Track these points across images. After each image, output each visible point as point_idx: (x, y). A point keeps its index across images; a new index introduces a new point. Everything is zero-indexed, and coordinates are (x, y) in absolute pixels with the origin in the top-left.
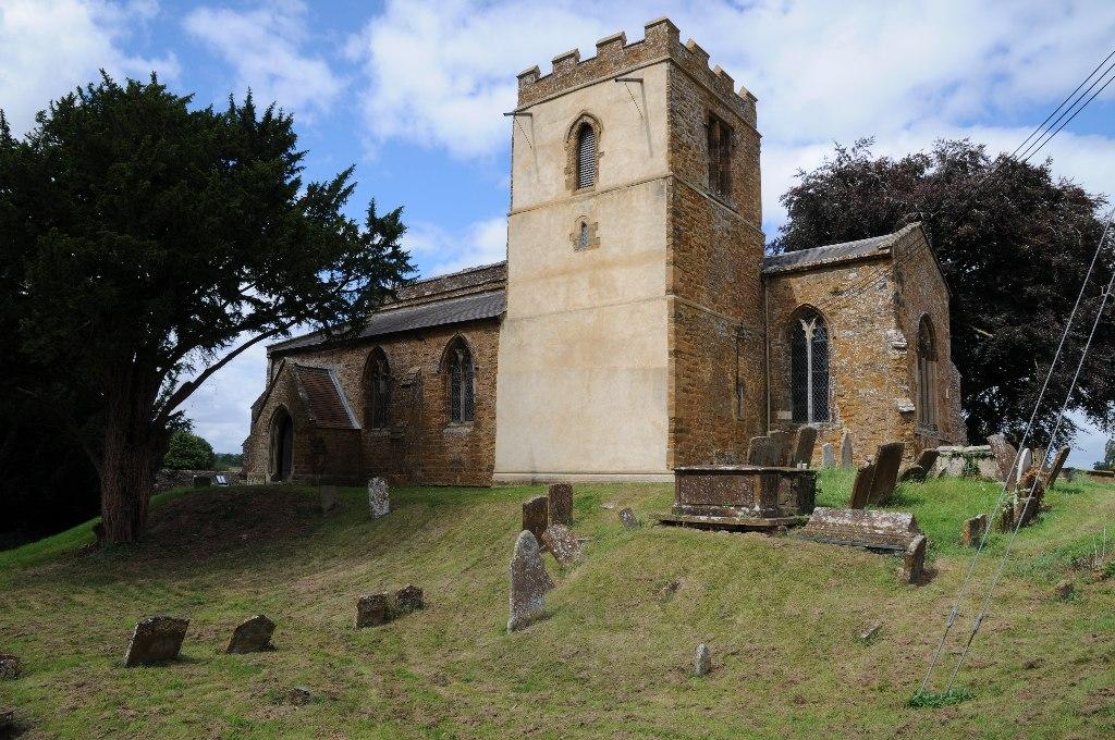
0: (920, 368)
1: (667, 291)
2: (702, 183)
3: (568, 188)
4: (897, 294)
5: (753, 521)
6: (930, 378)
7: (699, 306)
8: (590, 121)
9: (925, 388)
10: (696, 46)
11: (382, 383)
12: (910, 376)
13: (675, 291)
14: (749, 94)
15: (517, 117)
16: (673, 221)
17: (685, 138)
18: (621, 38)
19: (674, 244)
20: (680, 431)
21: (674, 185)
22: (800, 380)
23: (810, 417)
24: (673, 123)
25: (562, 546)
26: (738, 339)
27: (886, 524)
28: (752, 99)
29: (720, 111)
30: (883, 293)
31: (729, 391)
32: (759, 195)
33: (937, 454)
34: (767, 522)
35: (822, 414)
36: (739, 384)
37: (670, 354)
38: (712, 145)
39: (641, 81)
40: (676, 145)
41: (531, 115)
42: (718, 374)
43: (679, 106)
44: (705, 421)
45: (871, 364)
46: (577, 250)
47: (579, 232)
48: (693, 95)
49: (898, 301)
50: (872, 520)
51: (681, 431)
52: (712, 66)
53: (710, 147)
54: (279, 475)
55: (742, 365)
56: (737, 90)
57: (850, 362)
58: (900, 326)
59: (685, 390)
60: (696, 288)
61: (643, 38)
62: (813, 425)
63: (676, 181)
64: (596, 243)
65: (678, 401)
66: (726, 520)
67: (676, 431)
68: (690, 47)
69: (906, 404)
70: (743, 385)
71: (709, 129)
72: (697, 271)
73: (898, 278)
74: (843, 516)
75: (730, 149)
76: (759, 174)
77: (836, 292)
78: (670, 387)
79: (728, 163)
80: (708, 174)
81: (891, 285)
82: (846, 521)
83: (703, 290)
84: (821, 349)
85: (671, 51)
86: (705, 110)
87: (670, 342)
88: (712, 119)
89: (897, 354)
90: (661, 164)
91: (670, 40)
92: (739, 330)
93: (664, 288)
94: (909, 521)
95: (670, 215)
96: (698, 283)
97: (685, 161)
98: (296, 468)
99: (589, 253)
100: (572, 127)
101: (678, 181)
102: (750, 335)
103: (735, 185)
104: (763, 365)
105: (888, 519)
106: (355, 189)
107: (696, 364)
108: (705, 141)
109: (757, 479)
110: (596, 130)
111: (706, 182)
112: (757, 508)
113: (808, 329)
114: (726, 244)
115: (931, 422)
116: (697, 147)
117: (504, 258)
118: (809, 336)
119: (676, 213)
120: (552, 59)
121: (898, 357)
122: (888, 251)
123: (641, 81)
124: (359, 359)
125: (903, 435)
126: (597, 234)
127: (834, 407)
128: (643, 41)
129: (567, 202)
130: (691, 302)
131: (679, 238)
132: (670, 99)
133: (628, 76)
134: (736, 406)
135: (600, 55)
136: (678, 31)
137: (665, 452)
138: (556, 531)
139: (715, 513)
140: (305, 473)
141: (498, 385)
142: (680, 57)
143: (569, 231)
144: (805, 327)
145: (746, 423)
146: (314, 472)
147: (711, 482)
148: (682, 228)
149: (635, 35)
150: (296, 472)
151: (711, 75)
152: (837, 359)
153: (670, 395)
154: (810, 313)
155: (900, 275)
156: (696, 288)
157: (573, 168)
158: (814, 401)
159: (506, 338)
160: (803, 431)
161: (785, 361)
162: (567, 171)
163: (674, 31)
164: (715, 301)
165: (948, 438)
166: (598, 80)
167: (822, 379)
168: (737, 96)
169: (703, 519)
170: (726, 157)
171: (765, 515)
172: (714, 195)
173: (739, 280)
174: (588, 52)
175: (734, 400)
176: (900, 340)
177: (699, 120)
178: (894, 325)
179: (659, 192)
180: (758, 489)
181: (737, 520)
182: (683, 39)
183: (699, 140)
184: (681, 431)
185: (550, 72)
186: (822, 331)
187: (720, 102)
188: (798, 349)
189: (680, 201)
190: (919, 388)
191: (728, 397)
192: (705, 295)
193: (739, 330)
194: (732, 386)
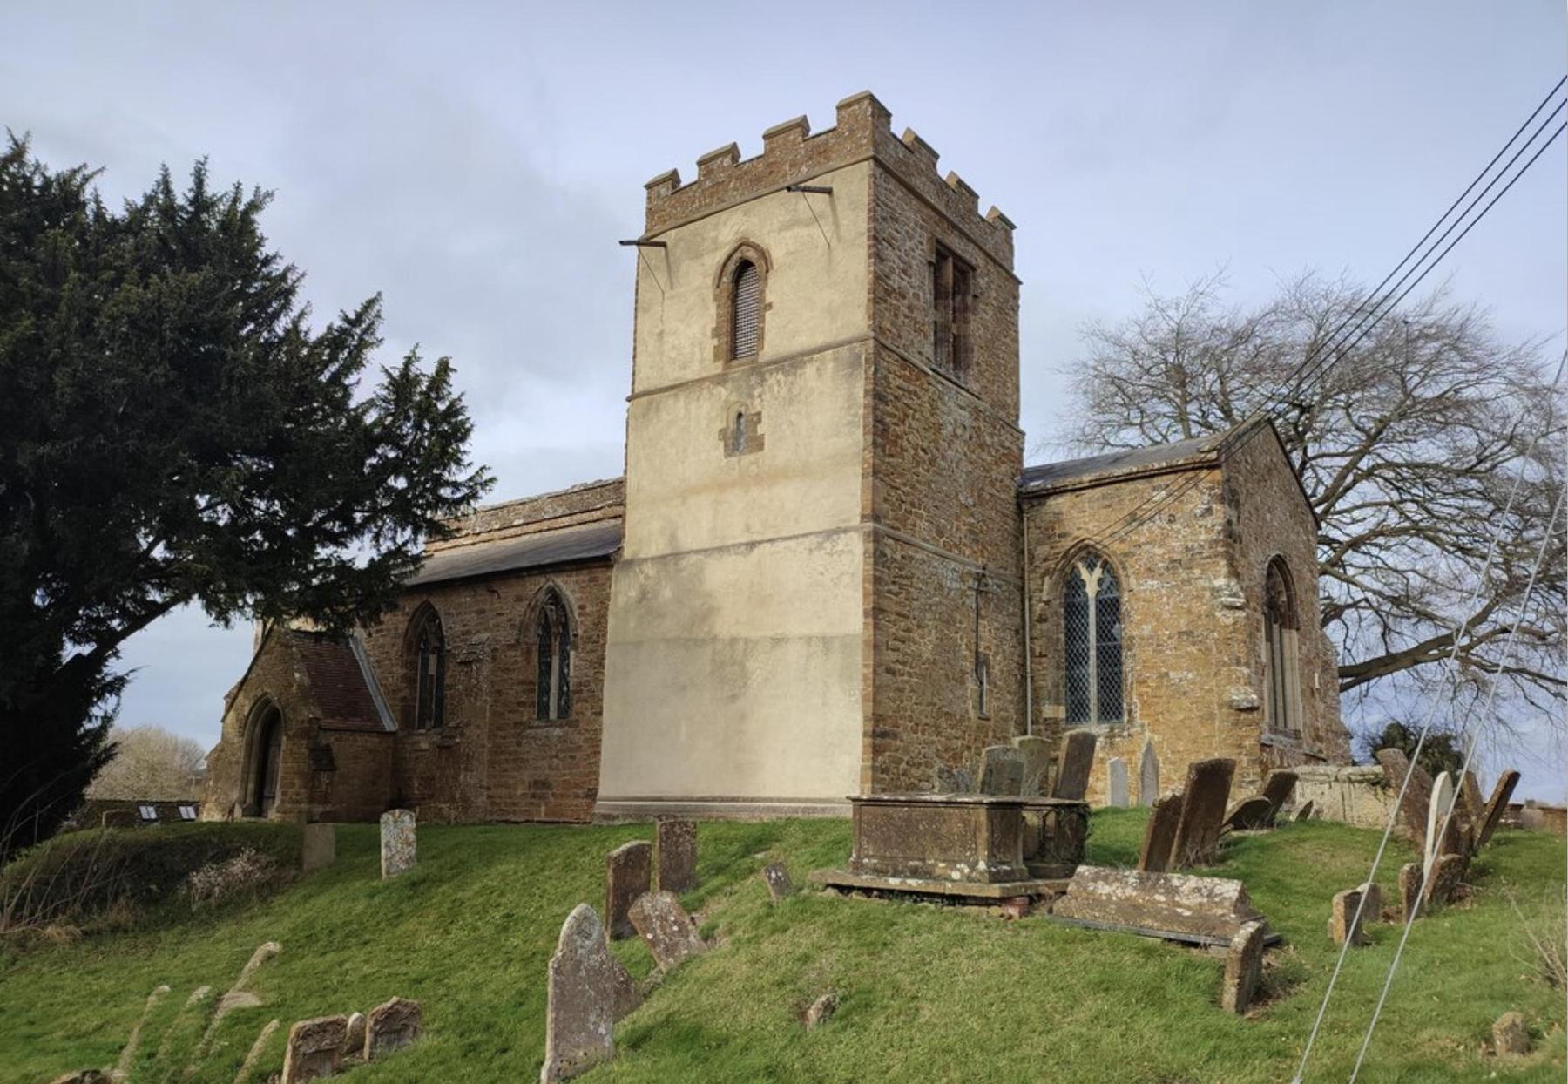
0: (1269, 639)
1: (863, 517)
2: (922, 350)
3: (716, 357)
4: (1229, 523)
5: (975, 890)
6: (1287, 655)
7: (914, 540)
8: (751, 254)
9: (1278, 671)
10: (917, 139)
11: (433, 659)
12: (1252, 650)
13: (876, 518)
14: (1002, 218)
15: (643, 248)
16: (875, 408)
17: (895, 282)
18: (802, 125)
19: (875, 444)
20: (880, 735)
21: (877, 354)
22: (1075, 658)
23: (1093, 714)
24: (877, 256)
25: (662, 927)
26: (979, 592)
27: (1196, 900)
28: (1004, 225)
29: (955, 242)
30: (1209, 521)
31: (964, 673)
32: (1015, 371)
33: (1293, 778)
34: (995, 891)
35: (1112, 708)
36: (980, 662)
37: (866, 614)
38: (939, 293)
39: (829, 192)
40: (882, 292)
41: (663, 245)
42: (946, 647)
43: (889, 229)
44: (925, 721)
45: (1189, 633)
46: (728, 454)
47: (732, 426)
48: (910, 213)
49: (1231, 535)
50: (1172, 891)
51: (884, 735)
52: (943, 171)
53: (936, 298)
54: (258, 805)
55: (984, 633)
56: (983, 211)
57: (1154, 630)
58: (1234, 573)
59: (890, 671)
60: (910, 512)
61: (835, 124)
62: (1094, 727)
63: (881, 346)
64: (757, 443)
65: (877, 689)
66: (932, 888)
67: (875, 735)
68: (907, 141)
69: (1242, 694)
70: (986, 662)
71: (936, 268)
72: (913, 487)
73: (1231, 497)
74: (1123, 882)
75: (970, 299)
76: (1016, 341)
77: (1133, 517)
78: (866, 666)
79: (967, 322)
80: (932, 339)
81: (1221, 512)
82: (1129, 892)
83: (921, 517)
84: (1110, 608)
85: (875, 144)
86: (929, 240)
87: (865, 596)
88: (942, 253)
89: (1226, 618)
90: (857, 320)
91: (875, 127)
92: (979, 578)
93: (858, 511)
94: (1235, 895)
95: (870, 400)
96: (913, 505)
97: (896, 315)
98: (284, 794)
99: (748, 459)
100: (725, 265)
101: (885, 347)
102: (999, 586)
103: (977, 356)
104: (1020, 631)
105: (1199, 890)
106: (101, 199)
107: (908, 630)
108: (929, 285)
109: (982, 811)
110: (759, 265)
111: (929, 350)
112: (982, 866)
113: (1091, 580)
114: (959, 445)
115: (1291, 726)
116: (916, 296)
117: (620, 474)
118: (1091, 589)
119: (878, 396)
120: (697, 158)
121: (1230, 621)
122: (1213, 455)
123: (829, 192)
124: (395, 622)
125: (1240, 746)
126: (760, 430)
127: (1133, 699)
128: (834, 129)
129: (720, 380)
130: (901, 534)
131: (883, 434)
132: (873, 219)
133: (808, 184)
134: (975, 696)
135: (769, 152)
136: (889, 115)
137: (858, 769)
138: (657, 903)
139: (915, 873)
140: (298, 802)
141: (607, 662)
142: (891, 155)
143: (720, 425)
144: (1084, 574)
145: (992, 723)
146: (311, 800)
147: (908, 820)
148: (888, 420)
149: (823, 120)
150: (283, 801)
151: (942, 186)
152: (1136, 627)
153: (865, 678)
154: (1090, 554)
155: (1234, 493)
156: (910, 512)
157: (726, 327)
158: (1101, 689)
159: (623, 589)
160: (1073, 739)
161: (1055, 628)
162: (716, 333)
163: (882, 114)
164: (941, 533)
165: (1320, 751)
166: (765, 191)
167: (1111, 657)
168: (983, 220)
169: (894, 883)
170: (961, 313)
171: (995, 878)
172: (942, 371)
173: (980, 502)
174: (752, 148)
175: (971, 685)
176: (1235, 595)
177: (918, 252)
178: (1224, 570)
179: (854, 364)
180: (984, 835)
181: (949, 888)
182: (898, 128)
183: (919, 285)
184: (884, 735)
185: (694, 178)
186: (1112, 581)
187: (954, 227)
188: (1073, 608)
189: (886, 378)
190: (1268, 672)
191: (962, 682)
192: (923, 524)
193: (979, 578)
194: (969, 666)
